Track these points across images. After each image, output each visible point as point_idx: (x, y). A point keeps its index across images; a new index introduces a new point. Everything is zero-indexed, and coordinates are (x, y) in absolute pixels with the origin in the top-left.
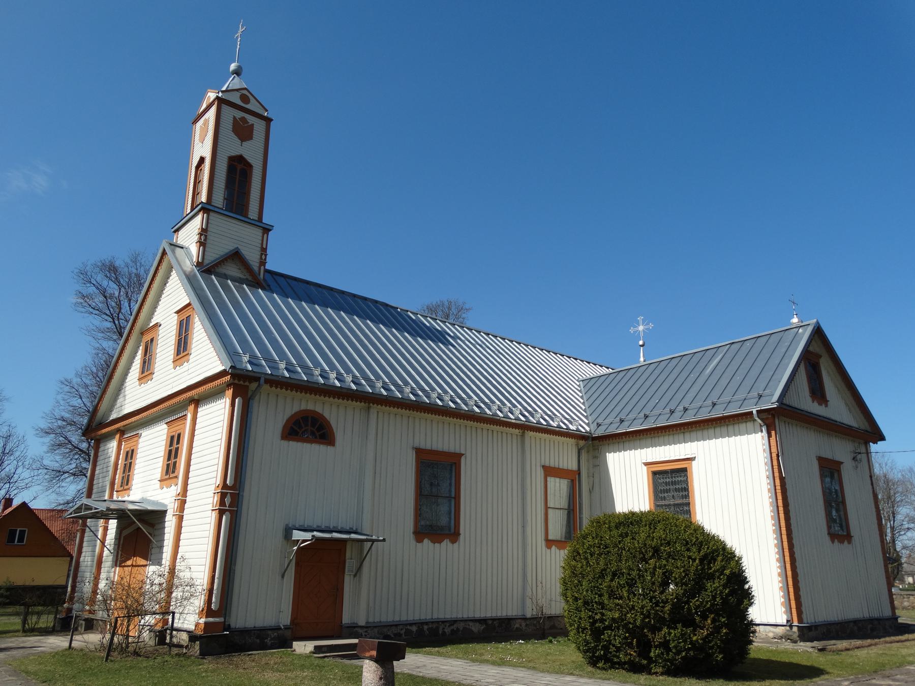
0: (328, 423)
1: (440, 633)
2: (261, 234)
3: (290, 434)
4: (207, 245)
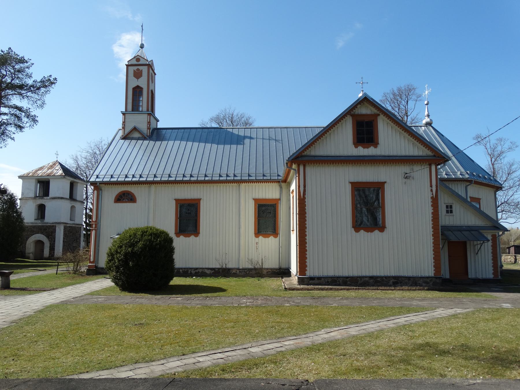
0: (133, 194)
1: (189, 273)
2: (147, 116)
3: (118, 200)
4: (125, 128)
